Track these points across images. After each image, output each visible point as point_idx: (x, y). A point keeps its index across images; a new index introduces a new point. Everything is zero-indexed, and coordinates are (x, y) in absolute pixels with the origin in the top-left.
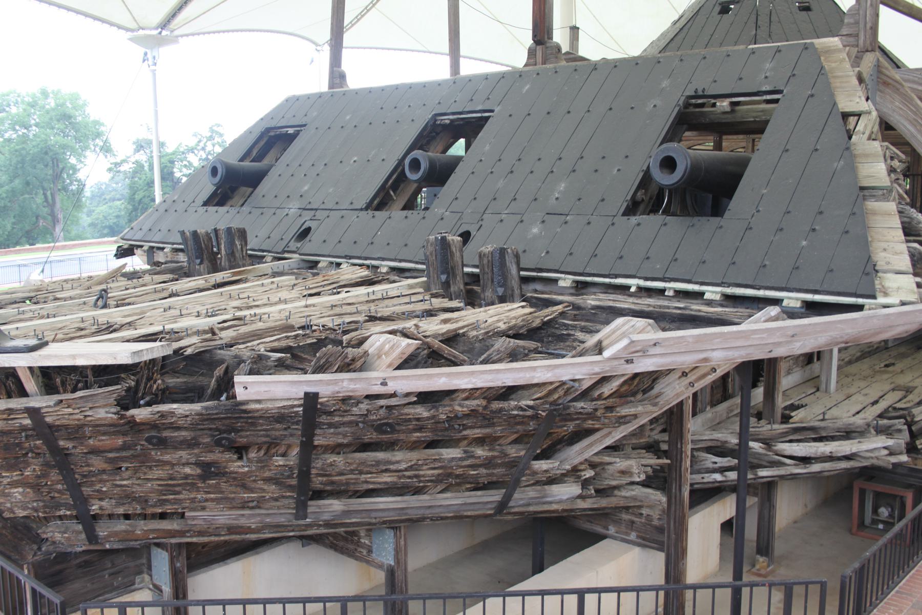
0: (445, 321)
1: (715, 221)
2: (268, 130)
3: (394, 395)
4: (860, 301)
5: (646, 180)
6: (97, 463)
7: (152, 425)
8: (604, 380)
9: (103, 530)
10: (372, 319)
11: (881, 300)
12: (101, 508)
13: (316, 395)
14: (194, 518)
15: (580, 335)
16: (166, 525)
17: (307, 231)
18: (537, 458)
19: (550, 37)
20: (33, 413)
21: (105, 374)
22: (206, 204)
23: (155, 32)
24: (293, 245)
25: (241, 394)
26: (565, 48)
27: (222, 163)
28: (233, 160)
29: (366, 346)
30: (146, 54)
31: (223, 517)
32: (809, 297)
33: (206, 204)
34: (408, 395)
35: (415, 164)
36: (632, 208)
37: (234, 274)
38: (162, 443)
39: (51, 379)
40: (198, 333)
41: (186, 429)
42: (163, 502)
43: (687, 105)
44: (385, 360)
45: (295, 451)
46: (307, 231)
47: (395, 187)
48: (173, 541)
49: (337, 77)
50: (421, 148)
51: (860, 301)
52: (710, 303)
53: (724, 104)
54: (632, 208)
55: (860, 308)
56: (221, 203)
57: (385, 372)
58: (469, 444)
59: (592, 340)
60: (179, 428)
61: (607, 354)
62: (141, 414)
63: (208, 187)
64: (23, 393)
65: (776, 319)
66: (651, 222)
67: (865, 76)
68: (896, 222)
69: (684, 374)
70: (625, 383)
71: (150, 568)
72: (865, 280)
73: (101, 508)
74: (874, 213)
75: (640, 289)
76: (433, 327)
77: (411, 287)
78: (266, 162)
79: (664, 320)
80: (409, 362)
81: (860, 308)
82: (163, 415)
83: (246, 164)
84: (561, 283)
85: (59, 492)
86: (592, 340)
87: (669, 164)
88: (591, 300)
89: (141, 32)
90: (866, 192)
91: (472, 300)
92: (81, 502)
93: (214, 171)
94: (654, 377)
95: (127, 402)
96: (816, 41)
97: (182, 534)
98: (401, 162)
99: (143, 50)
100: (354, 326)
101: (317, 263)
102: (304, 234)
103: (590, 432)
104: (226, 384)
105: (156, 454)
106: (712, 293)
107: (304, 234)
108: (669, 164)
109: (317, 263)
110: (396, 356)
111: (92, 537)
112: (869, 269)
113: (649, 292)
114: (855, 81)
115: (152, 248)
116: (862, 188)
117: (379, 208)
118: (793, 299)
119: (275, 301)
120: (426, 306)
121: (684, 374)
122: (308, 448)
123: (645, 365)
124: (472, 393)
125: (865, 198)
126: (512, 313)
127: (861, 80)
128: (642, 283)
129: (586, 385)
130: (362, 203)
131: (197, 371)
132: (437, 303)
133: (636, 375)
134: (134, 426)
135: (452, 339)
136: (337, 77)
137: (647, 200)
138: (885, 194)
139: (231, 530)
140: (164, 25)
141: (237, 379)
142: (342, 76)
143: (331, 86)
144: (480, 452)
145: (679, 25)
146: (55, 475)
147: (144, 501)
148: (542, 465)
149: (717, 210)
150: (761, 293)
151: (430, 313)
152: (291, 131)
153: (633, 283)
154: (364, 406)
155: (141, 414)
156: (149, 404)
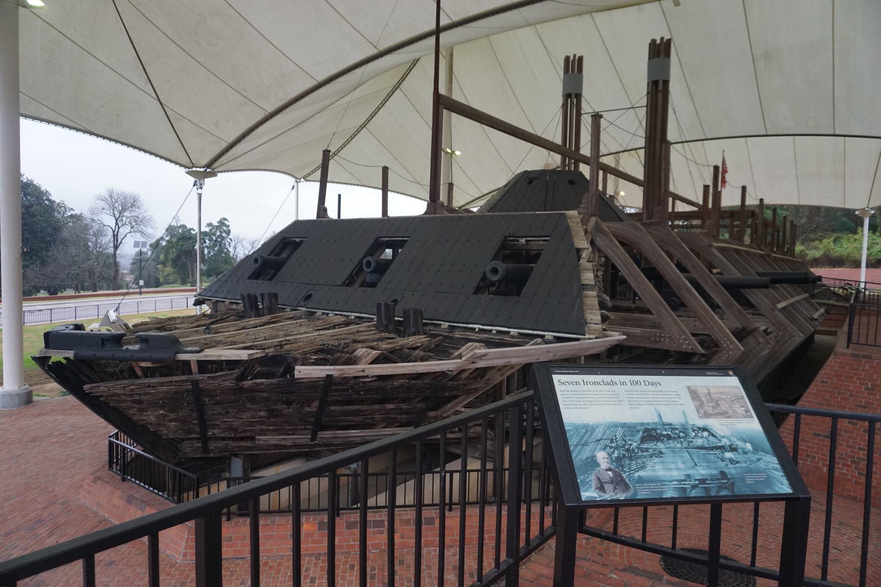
0: (390, 343)
1: (516, 298)
2: (284, 239)
3: (367, 377)
4: (579, 336)
5: (484, 278)
6: (218, 409)
7: (251, 390)
8: (463, 371)
9: (212, 445)
10: (355, 341)
11: (587, 336)
12: (213, 434)
13: (331, 376)
14: (260, 440)
15: (451, 351)
16: (243, 444)
17: (310, 295)
18: (431, 410)
19: (439, 198)
20: (195, 383)
21: (232, 364)
22: (249, 278)
23: (202, 170)
24: (303, 303)
25: (297, 375)
26: (446, 204)
27: (261, 256)
28: (265, 255)
29: (355, 353)
30: (196, 182)
31: (273, 439)
32: (557, 334)
33: (249, 278)
34: (373, 376)
35: (369, 264)
36: (477, 291)
37: (273, 318)
38: (253, 400)
39: (204, 366)
40: (274, 347)
41: (266, 392)
42: (244, 431)
43: (505, 240)
44: (364, 360)
45: (316, 404)
46: (310, 295)
47: (357, 274)
48: (246, 452)
49: (322, 209)
50: (370, 255)
51: (579, 336)
52: (513, 337)
53: (523, 241)
54: (477, 291)
55: (578, 339)
56: (257, 278)
57: (366, 367)
58: (399, 403)
59: (457, 353)
60: (262, 392)
61: (464, 359)
62: (247, 383)
63: (253, 267)
64: (190, 373)
65: (540, 344)
66: (486, 297)
67: (589, 230)
68: (595, 302)
69: (499, 370)
70: (472, 373)
71: (230, 468)
72: (580, 327)
73: (213, 434)
74: (587, 296)
75: (480, 329)
76: (384, 346)
77: (369, 327)
78: (284, 255)
79: (489, 344)
80: (375, 361)
81: (578, 339)
82: (258, 384)
83: (272, 257)
84: (443, 327)
85: (194, 424)
86: (457, 353)
87: (495, 271)
88: (458, 334)
89: (194, 169)
90: (584, 287)
91: (401, 334)
92: (204, 427)
93: (256, 261)
94: (485, 370)
95: (242, 378)
96: (566, 212)
97: (250, 448)
98: (361, 262)
99: (194, 179)
100: (346, 346)
101: (315, 313)
102: (308, 297)
103: (456, 397)
104: (290, 370)
105: (249, 405)
106: (514, 331)
107: (308, 297)
108: (495, 271)
109: (315, 313)
110: (370, 358)
111: (205, 448)
112: (583, 321)
113: (485, 331)
114: (583, 233)
115: (217, 301)
116: (583, 285)
117: (347, 285)
118: (549, 335)
119: (299, 332)
120: (377, 336)
121: (499, 370)
122: (324, 404)
123: (481, 364)
124: (402, 376)
125: (584, 289)
126: (419, 340)
127: (586, 232)
128: (481, 327)
129: (455, 373)
130: (340, 283)
131: (278, 363)
132: (384, 335)
133: (477, 369)
134: (242, 389)
135: (393, 351)
136: (322, 209)
137: (483, 286)
138: (592, 288)
139: (277, 446)
140: (209, 166)
141: (296, 367)
142: (325, 210)
143: (318, 216)
144: (403, 406)
145: (507, 188)
146: (195, 415)
147: (236, 430)
148: (432, 414)
149: (518, 293)
150: (535, 332)
151: (381, 339)
152: (298, 240)
153: (477, 326)
154: (352, 381)
155: (247, 383)
156: (251, 379)
